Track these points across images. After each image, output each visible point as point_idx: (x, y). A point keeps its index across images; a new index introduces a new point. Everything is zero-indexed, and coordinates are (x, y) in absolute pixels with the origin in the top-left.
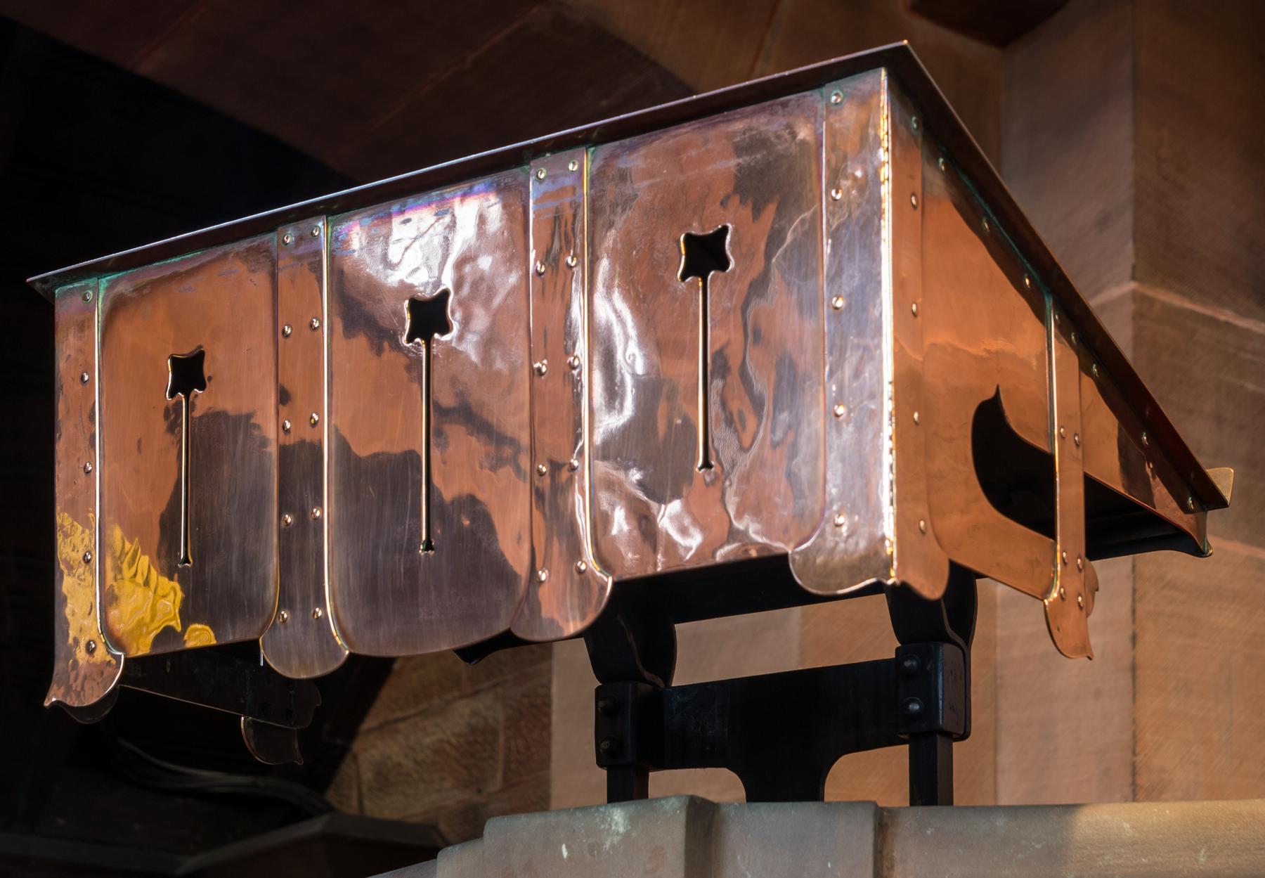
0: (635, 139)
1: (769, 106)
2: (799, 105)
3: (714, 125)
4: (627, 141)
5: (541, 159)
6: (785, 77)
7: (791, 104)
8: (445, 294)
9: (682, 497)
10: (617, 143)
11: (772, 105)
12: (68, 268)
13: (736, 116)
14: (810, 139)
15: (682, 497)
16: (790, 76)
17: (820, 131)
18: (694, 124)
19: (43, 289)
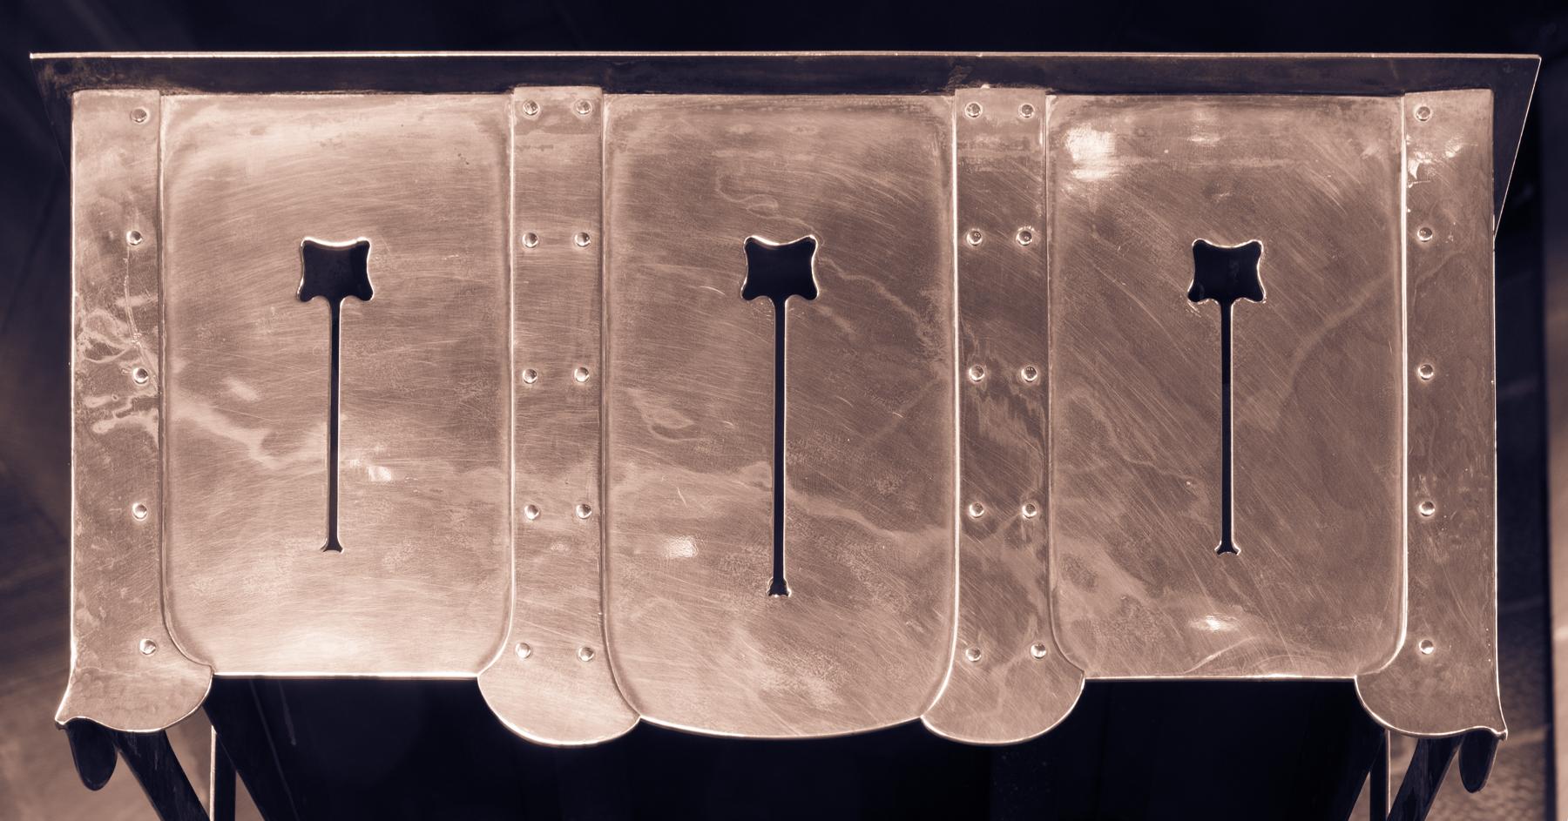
0: (1121, 99)
1: (1323, 102)
2: (1365, 112)
3: (1240, 107)
4: (1108, 99)
5: (975, 90)
6: (894, 57)
7: (1353, 107)
8: (807, 246)
9: (632, 548)
10: (1092, 98)
11: (1328, 102)
12: (717, 54)
13: (1275, 104)
14: (1382, 158)
15: (632, 548)
16: (899, 57)
17: (1397, 151)
18: (1213, 99)
19: (52, 84)
